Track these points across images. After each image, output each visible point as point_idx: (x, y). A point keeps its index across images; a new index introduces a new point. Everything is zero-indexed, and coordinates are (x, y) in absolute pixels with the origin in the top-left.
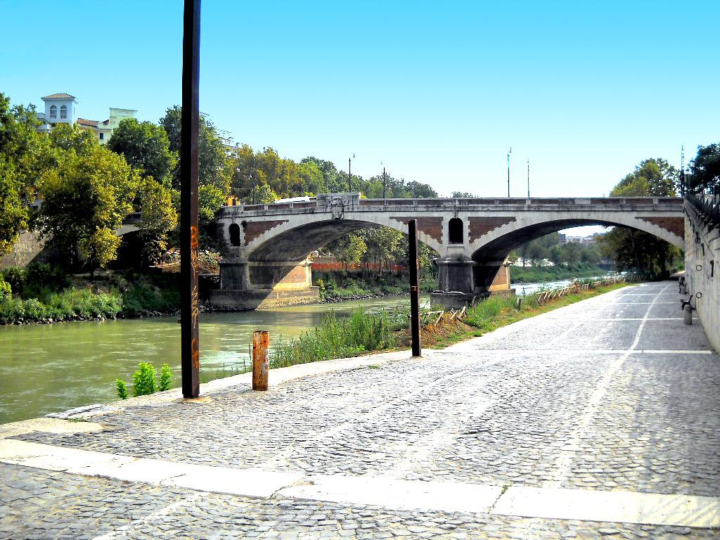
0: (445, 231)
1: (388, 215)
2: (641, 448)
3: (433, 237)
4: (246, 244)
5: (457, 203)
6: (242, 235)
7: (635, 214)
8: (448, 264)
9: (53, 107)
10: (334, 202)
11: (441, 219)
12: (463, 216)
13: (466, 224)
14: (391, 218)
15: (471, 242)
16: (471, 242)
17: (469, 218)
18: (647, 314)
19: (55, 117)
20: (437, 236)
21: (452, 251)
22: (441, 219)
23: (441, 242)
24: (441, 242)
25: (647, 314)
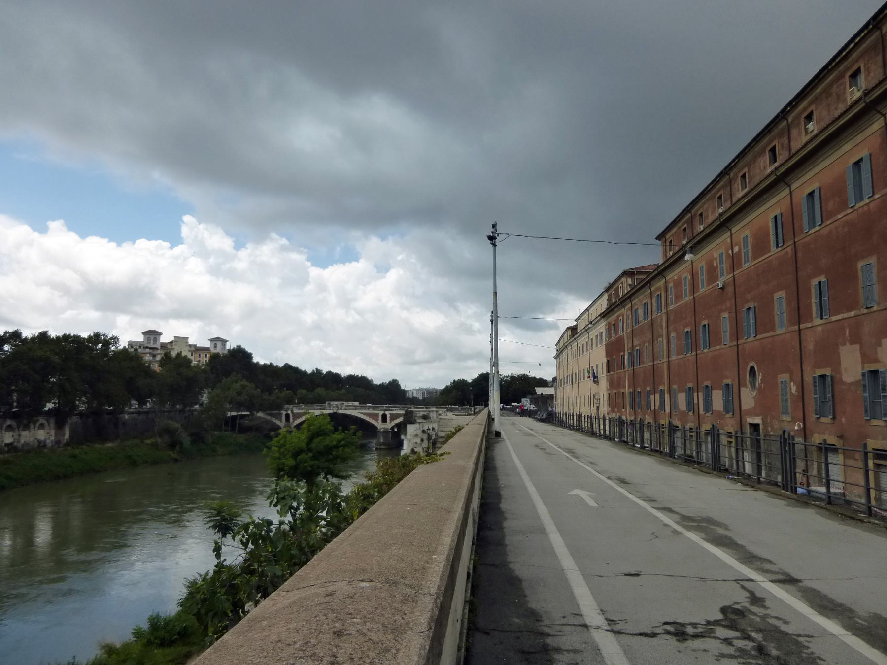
0: (380, 418)
1: (357, 411)
2: (359, 620)
3: (375, 420)
4: (293, 422)
5: (385, 408)
6: (291, 418)
7: (452, 413)
8: (57, 356)
9: (148, 338)
10: (335, 406)
11: (378, 414)
12: (387, 413)
13: (388, 416)
14: (359, 413)
15: (390, 423)
16: (390, 423)
17: (390, 414)
18: (274, 420)
19: (150, 343)
20: (377, 420)
21: (383, 426)
22: (378, 414)
23: (378, 422)
24: (378, 422)
25: (274, 420)
